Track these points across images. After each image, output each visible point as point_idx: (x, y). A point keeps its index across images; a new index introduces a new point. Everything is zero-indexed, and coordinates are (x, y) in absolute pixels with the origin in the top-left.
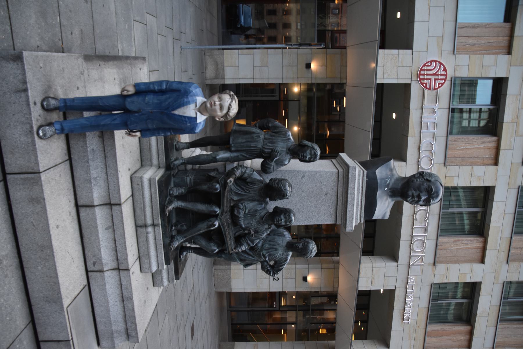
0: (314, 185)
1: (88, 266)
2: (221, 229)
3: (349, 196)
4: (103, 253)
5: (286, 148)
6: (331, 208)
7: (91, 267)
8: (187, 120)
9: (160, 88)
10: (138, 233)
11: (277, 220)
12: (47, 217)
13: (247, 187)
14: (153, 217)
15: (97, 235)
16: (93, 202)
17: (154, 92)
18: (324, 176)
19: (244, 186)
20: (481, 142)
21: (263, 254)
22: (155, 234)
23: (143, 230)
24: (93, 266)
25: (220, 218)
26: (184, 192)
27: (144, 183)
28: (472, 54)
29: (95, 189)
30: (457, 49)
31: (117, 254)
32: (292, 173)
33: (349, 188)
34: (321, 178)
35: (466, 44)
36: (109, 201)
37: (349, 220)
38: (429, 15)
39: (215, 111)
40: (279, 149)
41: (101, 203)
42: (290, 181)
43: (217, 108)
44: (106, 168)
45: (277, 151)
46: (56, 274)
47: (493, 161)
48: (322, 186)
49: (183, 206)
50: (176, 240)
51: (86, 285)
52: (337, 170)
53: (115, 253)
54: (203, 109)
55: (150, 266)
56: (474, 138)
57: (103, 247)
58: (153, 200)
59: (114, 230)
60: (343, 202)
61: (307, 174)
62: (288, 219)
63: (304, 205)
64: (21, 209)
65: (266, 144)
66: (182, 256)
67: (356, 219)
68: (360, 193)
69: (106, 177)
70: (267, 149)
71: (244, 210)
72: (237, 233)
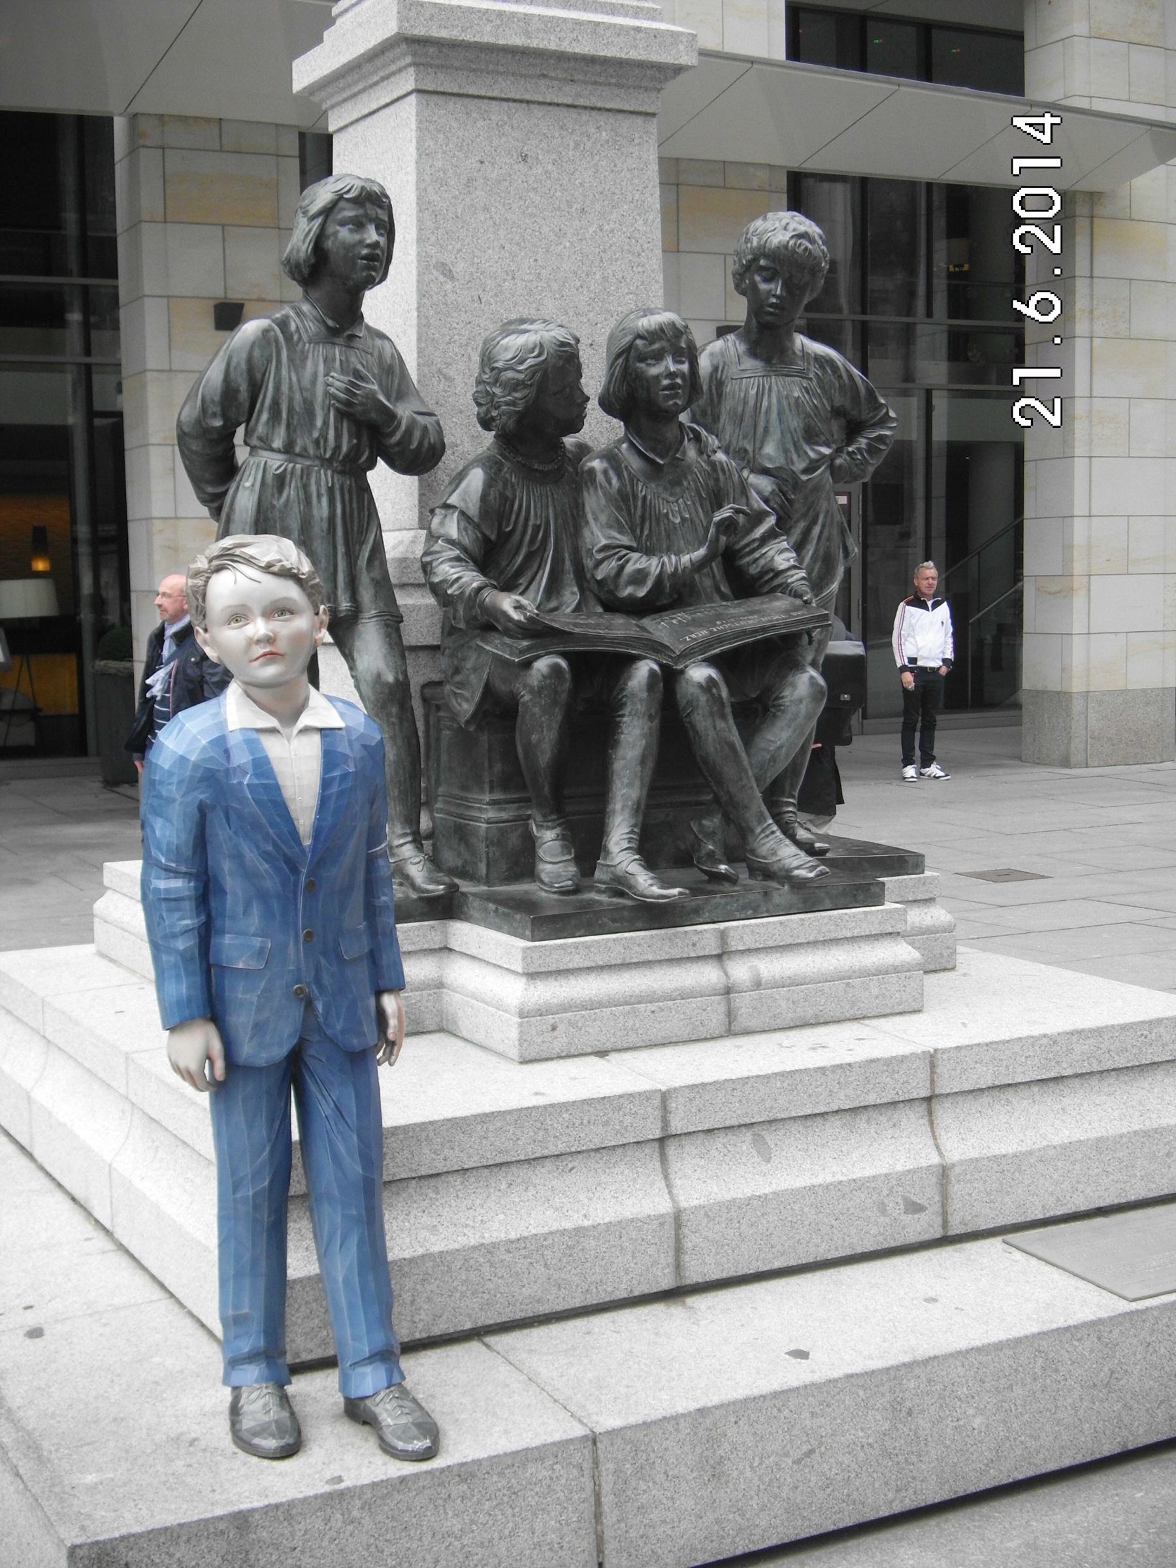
1: (926, 1237)
3: (534, 43)
4: (869, 1172)
5: (329, 347)
7: (925, 1226)
9: (188, 905)
11: (669, 397)
12: (776, 1395)
13: (522, 539)
14: (689, 959)
16: (661, 1219)
17: (206, 934)
18: (439, 164)
19: (517, 552)
22: (758, 950)
23: (744, 1002)
24: (923, 1215)
26: (558, 831)
31: (865, 1107)
32: (428, 325)
40: (338, 382)
41: (662, 1184)
42: (488, 327)
46: (999, 1347)
49: (635, 825)
50: (775, 859)
51: (1005, 1242)
52: (413, 99)
53: (864, 1116)
55: (896, 969)
57: (844, 1170)
58: (619, 961)
61: (433, 251)
62: (664, 344)
64: (743, 1516)
65: (317, 443)
66: (818, 845)
69: (548, 1164)
71: (624, 552)
72: (723, 589)
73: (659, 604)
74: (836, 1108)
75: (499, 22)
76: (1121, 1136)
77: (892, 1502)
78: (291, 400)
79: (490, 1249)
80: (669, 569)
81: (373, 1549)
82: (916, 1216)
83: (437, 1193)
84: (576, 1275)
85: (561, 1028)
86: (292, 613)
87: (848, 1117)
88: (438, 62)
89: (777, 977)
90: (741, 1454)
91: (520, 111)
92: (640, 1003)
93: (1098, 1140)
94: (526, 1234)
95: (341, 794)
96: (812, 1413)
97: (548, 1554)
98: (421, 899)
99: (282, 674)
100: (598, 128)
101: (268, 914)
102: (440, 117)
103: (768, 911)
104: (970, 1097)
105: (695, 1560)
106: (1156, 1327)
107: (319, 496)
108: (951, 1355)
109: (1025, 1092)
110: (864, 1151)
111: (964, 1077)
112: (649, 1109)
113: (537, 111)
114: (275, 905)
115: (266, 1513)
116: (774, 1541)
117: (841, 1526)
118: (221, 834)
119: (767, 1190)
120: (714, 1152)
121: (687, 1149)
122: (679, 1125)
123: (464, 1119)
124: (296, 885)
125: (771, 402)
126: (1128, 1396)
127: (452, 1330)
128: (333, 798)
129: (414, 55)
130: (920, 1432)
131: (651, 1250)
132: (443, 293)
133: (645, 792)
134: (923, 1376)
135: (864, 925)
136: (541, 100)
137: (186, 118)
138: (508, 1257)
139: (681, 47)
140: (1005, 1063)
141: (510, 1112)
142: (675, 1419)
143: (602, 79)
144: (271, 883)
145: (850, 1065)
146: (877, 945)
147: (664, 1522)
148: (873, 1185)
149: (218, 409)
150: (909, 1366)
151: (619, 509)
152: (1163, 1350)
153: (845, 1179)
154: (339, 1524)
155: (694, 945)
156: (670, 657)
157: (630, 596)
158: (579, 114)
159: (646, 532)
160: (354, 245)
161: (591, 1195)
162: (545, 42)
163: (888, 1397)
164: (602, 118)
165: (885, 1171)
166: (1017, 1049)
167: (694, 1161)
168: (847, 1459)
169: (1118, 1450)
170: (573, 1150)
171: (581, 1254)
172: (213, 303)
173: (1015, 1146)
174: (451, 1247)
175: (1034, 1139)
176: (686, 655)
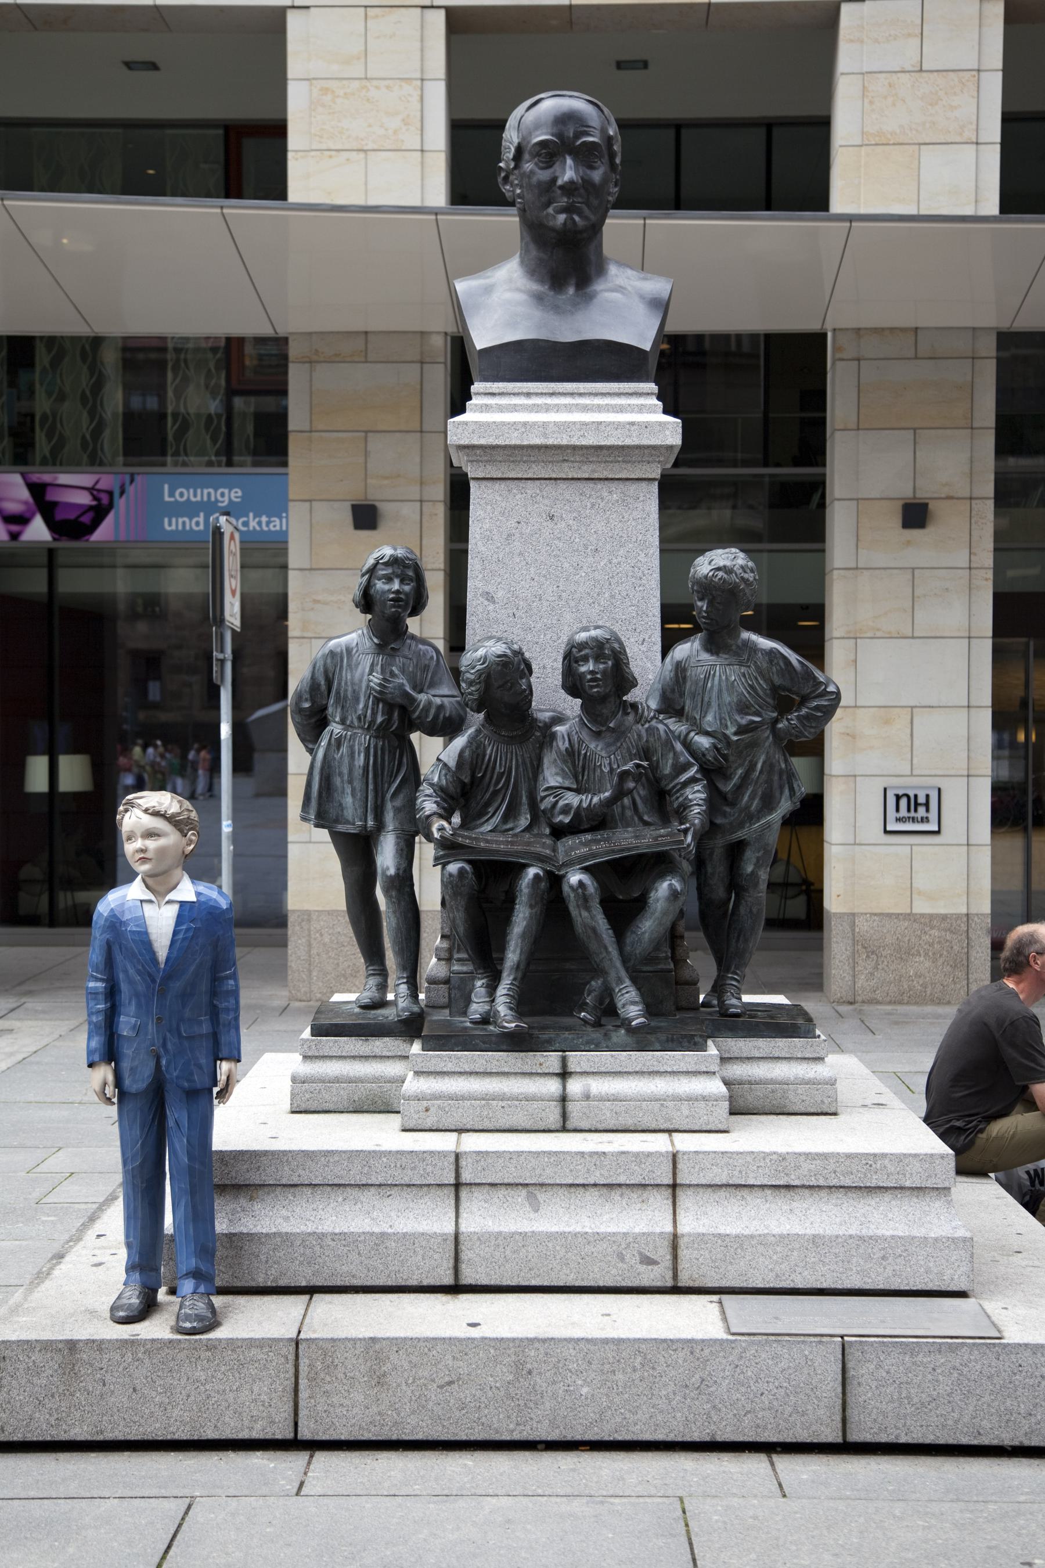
2: (607, 862)
3: (550, 442)
4: (612, 1229)
8: (184, 927)
9: (101, 997)
10: (587, 1127)
15: (550, 1236)
16: (444, 1237)
21: (735, 734)
23: (574, 1109)
24: (656, 1267)
29: (406, 1225)
31: (620, 1185)
33: (525, 443)
34: (495, 538)
36: (446, 1191)
37: (638, 437)
39: (161, 852)
43: (152, 844)
44: (344, 1185)
45: (380, 685)
46: (606, 1341)
48: (521, 534)
53: (619, 1191)
55: (705, 1098)
59: (542, 1185)
63: (589, 594)
64: (398, 1414)
65: (359, 718)
67: (641, 409)
68: (549, 401)
69: (373, 1190)
72: (646, 818)
73: (582, 828)
74: (592, 1182)
75: (523, 430)
76: (837, 1237)
77: (512, 1431)
79: (321, 1236)
80: (585, 805)
81: (149, 1379)
82: (650, 1267)
83: (295, 1197)
84: (381, 1263)
86: (159, 836)
87: (605, 1190)
89: (603, 1093)
90: (399, 1373)
91: (549, 487)
92: (494, 1100)
93: (814, 1236)
94: (346, 1231)
95: (184, 939)
96: (454, 1357)
97: (261, 1408)
98: (399, 1021)
99: (150, 870)
100: (610, 492)
101: (139, 1006)
102: (488, 495)
103: (607, 1047)
104: (710, 1190)
105: (362, 1435)
108: (565, 1339)
109: (759, 1193)
110: (614, 1216)
111: (701, 1175)
112: (446, 1163)
113: (562, 485)
114: (143, 1000)
115: (87, 1344)
116: (420, 1436)
117: (472, 1438)
118: (119, 957)
119: (528, 1229)
120: (496, 1200)
121: (475, 1194)
122: (468, 1177)
123: (313, 1152)
124: (154, 989)
125: (714, 684)
126: (717, 1401)
127: (293, 1285)
128: (179, 941)
129: (468, 455)
130: (537, 1387)
131: (436, 1256)
132: (486, 613)
133: (523, 957)
134: (541, 1349)
135: (682, 1064)
136: (565, 477)
137: (883, 329)
139: (667, 433)
140: (738, 1169)
141: (345, 1152)
142: (354, 1341)
143: (611, 459)
144: (141, 988)
145: (604, 1153)
147: (341, 1405)
148: (613, 1239)
149: (308, 696)
150: (531, 1341)
151: (564, 762)
152: (750, 1373)
153: (590, 1231)
154: (130, 1360)
155: (541, 1064)
156: (554, 865)
157: (561, 821)
158: (595, 484)
159: (585, 778)
161: (399, 1214)
162: (559, 440)
163: (513, 1357)
164: (613, 486)
165: (625, 1230)
166: (749, 1159)
167: (480, 1204)
169: (708, 1439)
170: (389, 1182)
171: (384, 1250)
172: (901, 503)
173: (740, 1229)
174: (294, 1231)
175: (758, 1228)
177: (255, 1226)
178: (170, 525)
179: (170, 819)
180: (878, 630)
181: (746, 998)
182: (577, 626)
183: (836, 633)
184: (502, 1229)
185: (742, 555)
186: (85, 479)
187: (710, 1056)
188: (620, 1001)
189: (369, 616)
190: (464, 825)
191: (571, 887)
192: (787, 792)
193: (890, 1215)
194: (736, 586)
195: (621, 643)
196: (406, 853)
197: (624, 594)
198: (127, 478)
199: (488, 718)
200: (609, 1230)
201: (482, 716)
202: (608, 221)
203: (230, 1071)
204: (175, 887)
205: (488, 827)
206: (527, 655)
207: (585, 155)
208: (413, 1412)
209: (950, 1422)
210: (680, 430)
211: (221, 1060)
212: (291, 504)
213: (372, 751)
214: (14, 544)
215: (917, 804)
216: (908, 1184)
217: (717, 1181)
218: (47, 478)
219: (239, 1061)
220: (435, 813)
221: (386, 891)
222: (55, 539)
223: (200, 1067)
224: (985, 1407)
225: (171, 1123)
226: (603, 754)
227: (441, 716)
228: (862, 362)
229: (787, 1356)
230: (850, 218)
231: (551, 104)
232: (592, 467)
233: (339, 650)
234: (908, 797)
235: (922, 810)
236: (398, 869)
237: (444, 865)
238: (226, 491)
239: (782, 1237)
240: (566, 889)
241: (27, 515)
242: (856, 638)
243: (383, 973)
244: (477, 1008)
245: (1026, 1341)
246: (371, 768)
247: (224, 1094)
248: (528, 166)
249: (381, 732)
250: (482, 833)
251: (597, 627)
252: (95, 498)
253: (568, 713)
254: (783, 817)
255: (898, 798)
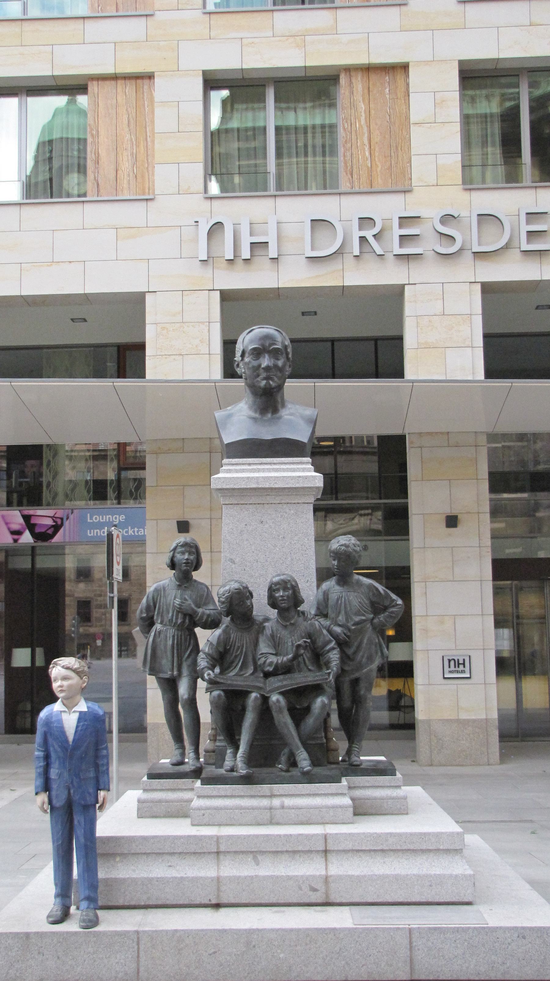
0: (245, 543)
3: (260, 486)
4: (296, 873)
6: (286, 513)
8: (82, 724)
9: (42, 760)
15: (265, 878)
16: (212, 879)
20: (353, 111)
21: (353, 625)
25: (268, 693)
26: (232, 750)
27: (201, 806)
28: (153, 156)
30: (144, 194)
35: (131, 174)
38: (70, 262)
39: (70, 686)
43: (65, 683)
47: (400, 77)
48: (248, 530)
54: (69, 705)
55: (341, 807)
56: (344, 129)
60: (274, 494)
63: (280, 558)
64: (189, 969)
67: (304, 470)
69: (177, 856)
70: (177, 619)
78: (163, 608)
79: (150, 880)
80: (280, 662)
82: (315, 893)
85: (206, 815)
88: (229, 494)
95: (81, 730)
106: (361, 935)
107: (170, 638)
118: (50, 740)
122: (224, 848)
129: (221, 493)
137: (432, 433)
138: (157, 883)
143: (290, 493)
144: (61, 755)
146: (335, 797)
151: (270, 641)
160: (181, 560)
168: (228, 958)
172: (444, 516)
176: (272, 691)
177: (118, 874)
178: (90, 533)
179: (75, 671)
180: (436, 577)
181: (362, 758)
182: (275, 574)
183: (416, 580)
184: (241, 874)
185: (353, 538)
186: (50, 513)
187: (343, 785)
188: (298, 759)
189: (174, 571)
190: (222, 672)
191: (273, 702)
192: (379, 654)
193: (433, 864)
194: (350, 553)
195: (296, 582)
196: (193, 688)
197: (298, 558)
198: (70, 511)
199: (232, 619)
200: (294, 874)
201: (229, 618)
202: (286, 384)
203: (105, 795)
204: (76, 705)
205: (232, 674)
206: (250, 589)
207: (275, 353)
208: (197, 967)
209: (464, 968)
210: (322, 479)
211: (100, 790)
212: (147, 521)
213: (176, 637)
214: (16, 544)
215: (459, 664)
216: (441, 847)
217: (347, 848)
218: (31, 512)
219: (109, 790)
220: (205, 667)
221: (183, 707)
222: (35, 542)
223: (89, 794)
224: (481, 960)
225: (76, 822)
226: (289, 636)
227: (210, 619)
228: (423, 449)
229: (382, 935)
230: (413, 382)
231: (259, 331)
232: (281, 497)
233: (159, 588)
234: (454, 660)
235: (461, 667)
236: (189, 695)
237: (211, 692)
238: (118, 516)
239: (380, 876)
240: (271, 703)
241: (22, 531)
242: (426, 582)
243: (183, 748)
244: (228, 763)
245: (500, 925)
246: (175, 646)
247: (101, 807)
248: (247, 360)
249: (180, 628)
250: (230, 677)
251: (284, 574)
252: (54, 521)
253: (272, 617)
254: (378, 666)
255: (449, 661)
